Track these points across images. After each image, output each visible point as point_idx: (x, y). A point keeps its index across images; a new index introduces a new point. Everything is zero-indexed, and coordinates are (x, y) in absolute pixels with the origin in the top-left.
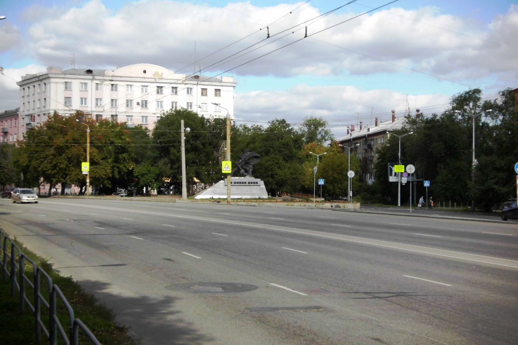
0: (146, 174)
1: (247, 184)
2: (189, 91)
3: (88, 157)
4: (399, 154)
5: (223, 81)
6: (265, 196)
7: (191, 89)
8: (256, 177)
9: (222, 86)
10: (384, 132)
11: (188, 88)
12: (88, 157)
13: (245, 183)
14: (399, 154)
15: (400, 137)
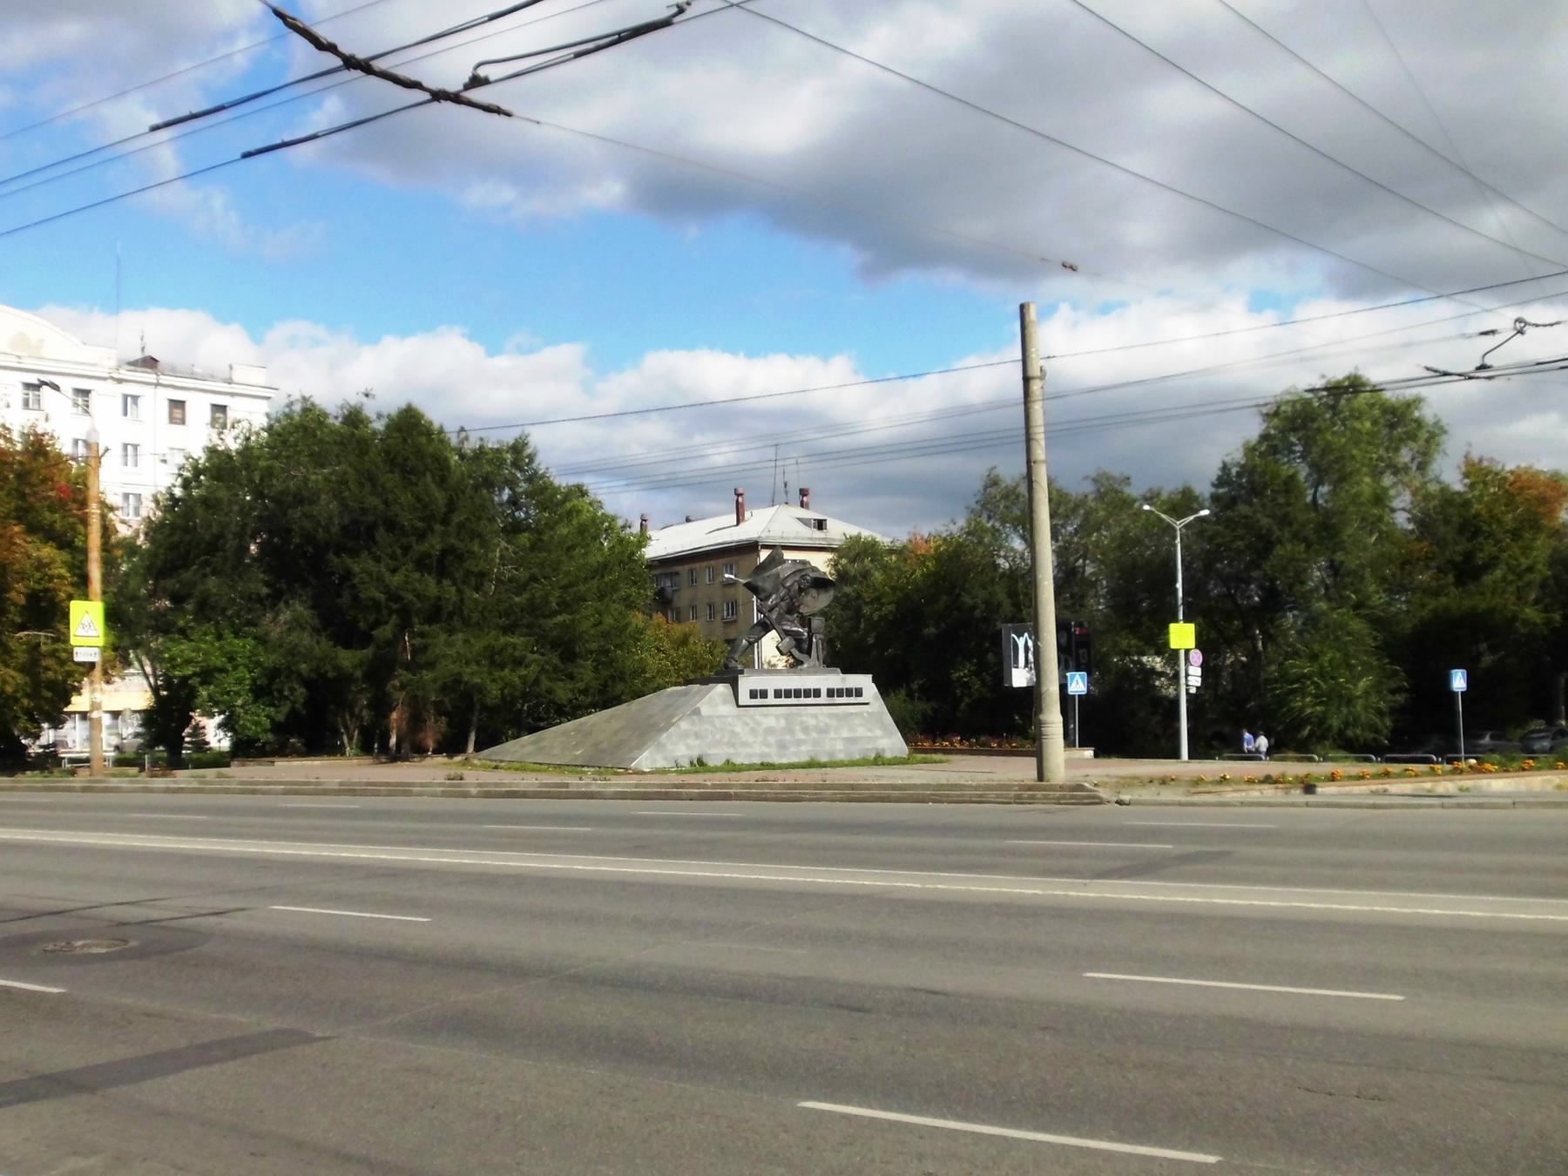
0: (223, 670)
1: (771, 699)
2: (130, 401)
3: (95, 572)
4: (1179, 585)
5: (235, 379)
6: (892, 742)
7: (135, 398)
8: (847, 670)
9: (233, 395)
10: (751, 547)
11: (125, 397)
12: (95, 572)
13: (817, 693)
14: (1179, 585)
15: (1179, 525)
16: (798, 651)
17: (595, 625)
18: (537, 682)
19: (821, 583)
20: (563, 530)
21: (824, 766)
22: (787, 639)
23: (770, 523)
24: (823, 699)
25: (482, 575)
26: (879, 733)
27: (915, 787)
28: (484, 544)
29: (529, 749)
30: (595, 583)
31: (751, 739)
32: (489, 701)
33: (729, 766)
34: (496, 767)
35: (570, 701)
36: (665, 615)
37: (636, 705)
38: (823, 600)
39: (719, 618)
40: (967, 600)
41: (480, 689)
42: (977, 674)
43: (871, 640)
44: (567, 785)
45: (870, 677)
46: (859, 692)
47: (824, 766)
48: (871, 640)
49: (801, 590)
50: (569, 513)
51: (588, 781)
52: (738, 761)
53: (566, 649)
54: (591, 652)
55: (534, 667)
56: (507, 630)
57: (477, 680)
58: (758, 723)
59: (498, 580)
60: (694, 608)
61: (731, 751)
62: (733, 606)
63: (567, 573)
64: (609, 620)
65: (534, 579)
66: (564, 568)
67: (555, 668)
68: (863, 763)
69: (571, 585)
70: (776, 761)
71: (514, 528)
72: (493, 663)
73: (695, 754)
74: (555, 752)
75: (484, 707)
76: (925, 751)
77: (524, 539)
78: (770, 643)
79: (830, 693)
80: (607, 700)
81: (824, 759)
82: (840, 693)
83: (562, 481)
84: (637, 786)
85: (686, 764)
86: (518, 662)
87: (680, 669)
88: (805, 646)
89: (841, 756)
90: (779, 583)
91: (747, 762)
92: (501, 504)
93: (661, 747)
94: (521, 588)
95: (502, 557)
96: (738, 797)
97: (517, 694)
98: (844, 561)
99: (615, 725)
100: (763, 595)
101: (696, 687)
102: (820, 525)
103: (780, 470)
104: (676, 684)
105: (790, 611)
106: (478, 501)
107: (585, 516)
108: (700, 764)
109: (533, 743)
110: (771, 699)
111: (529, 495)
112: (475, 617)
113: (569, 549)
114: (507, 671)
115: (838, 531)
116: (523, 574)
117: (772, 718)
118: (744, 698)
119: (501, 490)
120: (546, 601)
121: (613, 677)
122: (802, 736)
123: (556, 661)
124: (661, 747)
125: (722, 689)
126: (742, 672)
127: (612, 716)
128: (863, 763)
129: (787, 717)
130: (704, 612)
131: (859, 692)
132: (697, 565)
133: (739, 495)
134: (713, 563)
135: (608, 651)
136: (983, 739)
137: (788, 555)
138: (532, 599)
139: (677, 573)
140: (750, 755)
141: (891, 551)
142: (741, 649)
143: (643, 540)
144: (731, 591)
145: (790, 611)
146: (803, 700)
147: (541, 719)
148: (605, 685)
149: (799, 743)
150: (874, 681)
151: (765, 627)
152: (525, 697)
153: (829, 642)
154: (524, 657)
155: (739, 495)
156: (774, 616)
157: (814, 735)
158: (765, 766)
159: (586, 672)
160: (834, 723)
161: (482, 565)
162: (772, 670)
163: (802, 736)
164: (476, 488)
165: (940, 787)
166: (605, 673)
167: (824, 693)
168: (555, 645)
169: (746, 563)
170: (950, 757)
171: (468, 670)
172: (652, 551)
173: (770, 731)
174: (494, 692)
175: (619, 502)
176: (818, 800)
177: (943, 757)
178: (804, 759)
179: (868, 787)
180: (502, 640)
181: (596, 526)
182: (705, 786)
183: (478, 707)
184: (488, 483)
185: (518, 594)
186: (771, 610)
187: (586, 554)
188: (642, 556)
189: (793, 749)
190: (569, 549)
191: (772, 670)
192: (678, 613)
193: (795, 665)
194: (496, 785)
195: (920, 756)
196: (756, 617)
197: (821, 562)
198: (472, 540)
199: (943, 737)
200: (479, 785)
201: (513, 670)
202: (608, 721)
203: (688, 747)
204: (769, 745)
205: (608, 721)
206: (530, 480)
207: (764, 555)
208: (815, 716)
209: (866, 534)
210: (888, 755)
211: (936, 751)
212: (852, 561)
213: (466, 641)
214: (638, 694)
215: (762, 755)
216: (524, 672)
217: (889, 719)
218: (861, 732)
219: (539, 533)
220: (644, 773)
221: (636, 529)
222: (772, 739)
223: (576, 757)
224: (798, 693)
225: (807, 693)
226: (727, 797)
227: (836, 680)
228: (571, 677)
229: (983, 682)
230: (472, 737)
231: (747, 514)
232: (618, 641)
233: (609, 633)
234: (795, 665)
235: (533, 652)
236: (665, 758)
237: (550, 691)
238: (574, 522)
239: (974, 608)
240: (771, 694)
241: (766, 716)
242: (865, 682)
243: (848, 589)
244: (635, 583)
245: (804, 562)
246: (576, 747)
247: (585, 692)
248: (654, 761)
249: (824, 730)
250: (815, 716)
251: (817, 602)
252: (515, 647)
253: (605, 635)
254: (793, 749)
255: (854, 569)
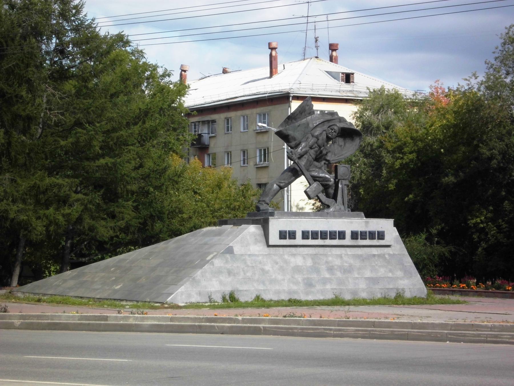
1: (299, 240)
6: (413, 283)
8: (371, 213)
10: (283, 98)
13: (342, 235)
16: (326, 194)
17: (136, 168)
18: (80, 220)
19: (347, 133)
20: (107, 78)
21: (347, 303)
22: (315, 185)
23: (303, 76)
24: (348, 241)
25: (29, 119)
26: (399, 273)
27: (433, 326)
28: (31, 89)
29: (71, 283)
30: (136, 129)
31: (280, 277)
32: (34, 237)
33: (259, 302)
34: (39, 301)
35: (112, 238)
36: (202, 160)
37: (172, 243)
38: (349, 149)
39: (251, 163)
40: (485, 151)
41: (26, 226)
42: (493, 220)
43: (392, 187)
44: (106, 318)
45: (391, 221)
46: (381, 235)
47: (347, 303)
48: (392, 187)
49: (328, 139)
50: (113, 62)
51: (127, 315)
52: (267, 297)
53: (109, 189)
54: (133, 193)
55: (77, 207)
56: (51, 171)
57: (23, 217)
58: (286, 262)
59: (44, 123)
60: (229, 154)
61: (261, 287)
62: (265, 153)
63: (111, 119)
64: (149, 164)
65: (78, 124)
66: (109, 115)
67: (98, 206)
68: (385, 301)
69: (114, 130)
70: (303, 297)
71: (61, 75)
72: (38, 202)
73: (228, 289)
74: (96, 287)
75: (29, 243)
76: (443, 292)
77: (70, 86)
78: (299, 186)
79: (355, 235)
80: (146, 237)
81: (347, 297)
82: (363, 235)
83: (106, 28)
84: (172, 319)
85: (218, 299)
86: (64, 201)
87: (214, 211)
88: (331, 191)
89: (364, 295)
90: (308, 130)
91: (275, 298)
92: (47, 53)
93: (196, 282)
94: (67, 132)
95: (48, 102)
96: (266, 331)
97: (60, 231)
98: (368, 113)
99: (154, 261)
100: (293, 144)
101: (228, 228)
102: (348, 78)
103: (311, 26)
104: (210, 224)
105: (318, 159)
106: (26, 49)
107: (128, 67)
108: (231, 300)
109: (73, 278)
110: (299, 240)
111: (76, 43)
112: (21, 160)
113: (112, 96)
114: (51, 210)
115: (364, 84)
116: (69, 119)
117: (300, 258)
118: (274, 238)
119: (49, 39)
120: (89, 145)
121: (152, 217)
122: (327, 276)
123: (98, 200)
124: (196, 282)
125: (253, 229)
126: (272, 214)
127: (151, 254)
128: (385, 301)
129: (314, 257)
130: (238, 157)
131: (381, 235)
132: (232, 114)
133: (272, 49)
134: (247, 112)
135: (148, 193)
136: (498, 282)
137: (317, 106)
138: (76, 143)
139: (214, 121)
140: (278, 292)
141: (413, 104)
142: (272, 193)
143: (182, 88)
144: (265, 138)
145: (318, 159)
146: (328, 242)
147: (84, 256)
148: (145, 224)
149: (325, 281)
150: (396, 225)
151: (294, 173)
152: (68, 234)
153: (354, 188)
154: (68, 197)
155: (272, 49)
156: (303, 163)
157: (339, 274)
158: (293, 303)
159: (127, 212)
160: (357, 263)
161: (29, 110)
162: (301, 214)
163: (327, 276)
164: (24, 37)
165: (457, 326)
166: (145, 213)
167: (348, 235)
168: (97, 187)
169: (279, 114)
170: (466, 299)
171: (15, 208)
172: (190, 100)
173: (297, 269)
174: (39, 227)
175: (160, 52)
176: (341, 336)
177: (461, 298)
178: (330, 296)
179: (389, 325)
180: (48, 181)
181: (136, 73)
182: (236, 321)
183: (22, 243)
184: (37, 32)
185: (65, 138)
186: (301, 157)
187: (129, 101)
188: (181, 104)
189: (319, 287)
190: (112, 96)
191: (301, 214)
192: (214, 159)
193: (322, 210)
194: (38, 317)
195: (438, 297)
196: (287, 163)
197: (348, 113)
198: (20, 85)
199: (461, 278)
200: (22, 317)
201: (57, 209)
202: (147, 258)
203: (221, 283)
204: (297, 283)
205: (147, 258)
206: (76, 30)
207: (295, 105)
208: (336, 256)
209: (390, 87)
210: (408, 295)
211: (453, 292)
212: (377, 112)
213: (13, 181)
214: (176, 233)
215: (290, 292)
216: (67, 211)
217: (409, 261)
218: (382, 272)
219: (85, 80)
220: (179, 307)
221: (175, 78)
222: (299, 278)
223: (116, 291)
224: (324, 235)
225: (333, 235)
226: (256, 331)
227: (359, 223)
228: (113, 216)
229: (499, 227)
230: (17, 271)
231: (280, 67)
232: (158, 183)
233: (148, 176)
234: (322, 210)
235: (76, 192)
236: (200, 294)
237: (92, 229)
238: (118, 70)
239: (491, 158)
240: (299, 235)
241: (294, 255)
242: (386, 225)
243: (370, 139)
244: (175, 130)
245: (333, 114)
246: (116, 282)
247: (126, 230)
248: (189, 296)
249: (348, 270)
250: (340, 256)
251: (343, 151)
252: (60, 186)
253: (146, 177)
254: (319, 287)
255: (376, 121)
